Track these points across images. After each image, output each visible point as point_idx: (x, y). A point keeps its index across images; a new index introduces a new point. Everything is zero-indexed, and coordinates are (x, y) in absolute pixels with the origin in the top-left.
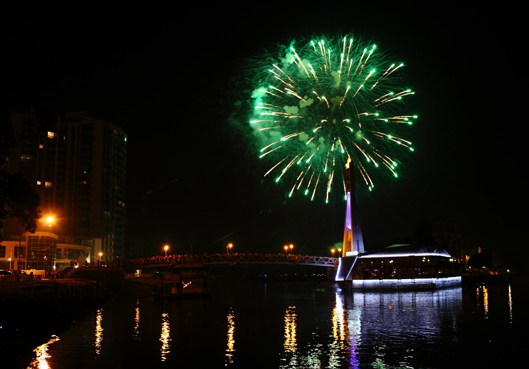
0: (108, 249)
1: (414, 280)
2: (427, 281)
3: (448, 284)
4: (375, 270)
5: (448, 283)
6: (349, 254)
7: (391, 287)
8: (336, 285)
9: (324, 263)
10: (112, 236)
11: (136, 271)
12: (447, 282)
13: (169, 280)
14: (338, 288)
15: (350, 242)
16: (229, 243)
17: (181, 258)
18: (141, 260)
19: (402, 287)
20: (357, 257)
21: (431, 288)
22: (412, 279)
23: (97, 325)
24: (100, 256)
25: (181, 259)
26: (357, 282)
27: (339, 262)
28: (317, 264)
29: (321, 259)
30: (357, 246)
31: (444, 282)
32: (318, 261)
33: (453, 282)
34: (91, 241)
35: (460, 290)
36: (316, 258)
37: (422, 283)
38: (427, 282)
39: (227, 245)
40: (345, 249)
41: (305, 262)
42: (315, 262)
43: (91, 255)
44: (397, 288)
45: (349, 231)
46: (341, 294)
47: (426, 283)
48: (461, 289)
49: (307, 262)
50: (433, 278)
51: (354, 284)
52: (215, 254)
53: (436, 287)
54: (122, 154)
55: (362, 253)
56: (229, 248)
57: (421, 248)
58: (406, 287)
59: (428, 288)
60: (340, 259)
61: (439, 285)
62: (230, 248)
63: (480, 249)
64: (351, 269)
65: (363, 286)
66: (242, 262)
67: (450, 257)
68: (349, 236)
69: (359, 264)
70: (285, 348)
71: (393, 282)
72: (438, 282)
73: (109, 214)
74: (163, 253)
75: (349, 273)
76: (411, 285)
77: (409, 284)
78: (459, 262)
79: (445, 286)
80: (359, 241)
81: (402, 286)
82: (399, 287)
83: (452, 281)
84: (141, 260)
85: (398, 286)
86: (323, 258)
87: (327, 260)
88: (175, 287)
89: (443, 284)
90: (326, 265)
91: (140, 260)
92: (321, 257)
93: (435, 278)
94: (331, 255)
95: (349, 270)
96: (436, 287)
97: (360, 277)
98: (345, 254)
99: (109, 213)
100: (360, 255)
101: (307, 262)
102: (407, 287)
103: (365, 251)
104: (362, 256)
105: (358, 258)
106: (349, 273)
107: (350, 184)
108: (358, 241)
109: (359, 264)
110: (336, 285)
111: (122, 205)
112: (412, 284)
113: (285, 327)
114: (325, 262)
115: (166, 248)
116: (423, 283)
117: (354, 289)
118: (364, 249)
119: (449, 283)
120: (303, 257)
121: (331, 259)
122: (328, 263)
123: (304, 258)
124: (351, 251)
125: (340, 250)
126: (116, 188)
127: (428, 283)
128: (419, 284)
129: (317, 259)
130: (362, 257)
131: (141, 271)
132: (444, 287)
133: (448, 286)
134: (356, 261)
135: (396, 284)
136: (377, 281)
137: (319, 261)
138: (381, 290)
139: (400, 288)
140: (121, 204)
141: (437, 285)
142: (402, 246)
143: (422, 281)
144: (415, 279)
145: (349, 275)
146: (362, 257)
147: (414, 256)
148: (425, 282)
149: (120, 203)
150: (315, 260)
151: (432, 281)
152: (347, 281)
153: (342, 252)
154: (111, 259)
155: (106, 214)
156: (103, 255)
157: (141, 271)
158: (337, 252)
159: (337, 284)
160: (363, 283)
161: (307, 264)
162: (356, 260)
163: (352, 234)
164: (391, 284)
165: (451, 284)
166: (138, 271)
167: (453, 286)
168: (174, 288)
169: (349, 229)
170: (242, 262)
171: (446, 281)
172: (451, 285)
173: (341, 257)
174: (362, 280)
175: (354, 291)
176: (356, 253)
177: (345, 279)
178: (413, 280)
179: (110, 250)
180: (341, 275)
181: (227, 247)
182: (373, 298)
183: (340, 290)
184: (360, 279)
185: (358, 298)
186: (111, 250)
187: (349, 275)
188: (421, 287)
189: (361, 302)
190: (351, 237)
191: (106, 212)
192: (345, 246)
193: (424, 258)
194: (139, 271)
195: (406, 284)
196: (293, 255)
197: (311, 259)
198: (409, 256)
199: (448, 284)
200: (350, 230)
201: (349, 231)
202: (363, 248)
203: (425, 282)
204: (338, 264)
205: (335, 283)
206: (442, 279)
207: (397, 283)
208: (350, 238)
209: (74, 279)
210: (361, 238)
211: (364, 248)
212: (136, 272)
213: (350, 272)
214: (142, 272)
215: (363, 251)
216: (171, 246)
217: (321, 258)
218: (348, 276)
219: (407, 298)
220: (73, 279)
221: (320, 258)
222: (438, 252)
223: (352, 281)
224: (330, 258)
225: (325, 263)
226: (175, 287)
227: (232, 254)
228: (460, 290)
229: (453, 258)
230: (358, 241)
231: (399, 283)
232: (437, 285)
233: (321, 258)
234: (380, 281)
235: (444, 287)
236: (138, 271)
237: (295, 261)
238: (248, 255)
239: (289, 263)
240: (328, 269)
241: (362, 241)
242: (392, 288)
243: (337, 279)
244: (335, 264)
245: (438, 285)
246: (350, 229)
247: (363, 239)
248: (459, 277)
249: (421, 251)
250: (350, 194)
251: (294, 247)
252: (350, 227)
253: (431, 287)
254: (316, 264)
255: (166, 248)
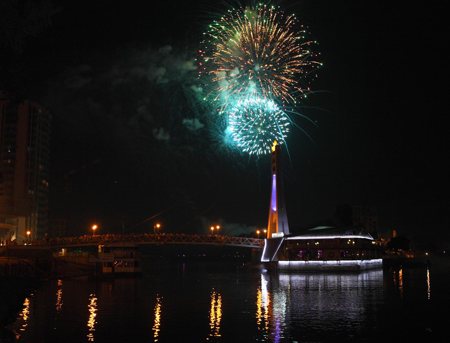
0: (32, 228)
1: (339, 262)
2: (352, 262)
3: (371, 266)
4: (300, 252)
5: (371, 265)
6: (274, 235)
7: (317, 268)
8: (262, 266)
9: (250, 244)
10: (35, 215)
11: (62, 250)
12: (370, 264)
13: (103, 259)
14: (264, 269)
15: (275, 224)
16: (157, 223)
17: (109, 237)
18: (69, 239)
19: (327, 269)
20: (283, 239)
21: (356, 270)
22: (337, 260)
23: (26, 302)
24: (28, 235)
25: (110, 238)
26: (283, 263)
27: (264, 243)
28: (242, 245)
29: (256, 241)
30: (282, 228)
31: (367, 264)
32: (244, 242)
33: (375, 264)
34: (15, 220)
35: (381, 273)
36: (242, 239)
37: (347, 265)
38: (353, 263)
39: (155, 225)
40: (270, 230)
41: (231, 243)
42: (241, 243)
43: (16, 234)
44: (322, 269)
45: (274, 213)
46: (266, 275)
47: (351, 264)
48: (382, 272)
49: (233, 243)
50: (358, 260)
51: (280, 265)
52: (143, 234)
53: (361, 269)
54: (46, 133)
55: (287, 234)
56: (156, 228)
57: (347, 231)
58: (331, 269)
59: (353, 270)
60: (265, 240)
61: (363, 267)
62: (212, 230)
63: (395, 232)
64: (277, 250)
65: (289, 267)
66: (169, 243)
67: (373, 239)
68: (274, 218)
69: (285, 245)
70: (265, 320)
71: (319, 263)
72: (362, 264)
73: (33, 193)
74: (92, 232)
75: (275, 254)
76: (336, 266)
77: (335, 265)
78: (380, 245)
79: (369, 268)
80: (284, 223)
81: (328, 268)
82: (324, 268)
83: (375, 263)
84: (69, 239)
85: (323, 268)
86: (248, 239)
87: (251, 241)
88: (107, 266)
89: (366, 266)
90: (251, 246)
91: (68, 239)
92: (247, 238)
93: (360, 260)
94: (255, 236)
95: (275, 251)
96: (361, 269)
97: (286, 258)
98: (271, 235)
99: (33, 192)
100: (286, 236)
101: (233, 243)
102: (332, 268)
103: (290, 233)
104: (288, 238)
105: (284, 239)
106: (275, 254)
107: (276, 168)
108: (283, 222)
109: (285, 245)
110: (262, 266)
111: (46, 184)
112: (337, 265)
113: (89, 318)
114: (250, 243)
115: (95, 227)
116: (348, 265)
117: (279, 269)
118: (289, 231)
119: (372, 265)
120: (229, 238)
121: (256, 240)
122: (253, 244)
123: (230, 239)
124: (276, 233)
125: (265, 231)
126: (40, 168)
127: (353, 264)
128: (344, 266)
129: (243, 241)
130: (289, 238)
131: (66, 249)
132: (368, 269)
133: (371, 268)
134: (282, 243)
135: (321, 266)
136: (303, 262)
137: (245, 242)
138: (307, 271)
139: (325, 269)
140: (45, 183)
141: (361, 267)
142: (313, 228)
143: (347, 263)
144: (341, 261)
145: (274, 256)
146: (289, 238)
147: (340, 238)
148: (350, 264)
149: (44, 182)
150: (241, 241)
151: (357, 263)
152: (273, 262)
153: (267, 234)
154: (34, 237)
155: (30, 193)
156: (30, 233)
157: (66, 249)
158: (262, 233)
159: (262, 265)
160: (289, 264)
161: (233, 244)
162: (282, 242)
163: (277, 216)
164: (316, 265)
165: (373, 266)
166: (63, 250)
167: (375, 268)
168: (106, 267)
169: (274, 211)
170: (169, 243)
171: (369, 263)
172: (373, 267)
173: (266, 239)
174: (288, 261)
175: (279, 272)
176: (282, 235)
177: (270, 260)
178: (338, 262)
179: (33, 229)
180: (266, 257)
181: (155, 227)
182: (298, 279)
183: (266, 271)
184: (286, 260)
185: (284, 278)
186: (35, 229)
187: (274, 256)
188: (346, 269)
189: (287, 284)
190: (276, 219)
191: (30, 191)
192: (270, 227)
193: (350, 241)
194: (64, 250)
195: (331, 266)
196: (220, 236)
197: (237, 240)
198: (335, 238)
199: (371, 266)
200: (275, 212)
201: (274, 213)
202: (288, 229)
203: (350, 264)
204: (264, 245)
205: (261, 264)
206: (366, 261)
207: (323, 265)
208: (276, 220)
209: (5, 257)
210: (286, 220)
211: (289, 230)
212: (62, 251)
213: (276, 253)
214: (67, 252)
215: (288, 233)
216: (99, 226)
217: (237, 239)
218: (274, 257)
219: (332, 279)
220: (3, 257)
221: (245, 239)
222: (362, 235)
223: (278, 261)
224: (255, 239)
225: (251, 244)
226: (107, 266)
227: (160, 234)
228: (381, 273)
229: (375, 241)
230: (283, 222)
231: (325, 265)
232: (361, 267)
233: (247, 239)
234: (306, 263)
235: (368, 269)
236: (63, 250)
237: (221, 242)
238: (175, 235)
239: (216, 244)
240: (253, 250)
241: (287, 223)
242: (318, 269)
243: (262, 260)
244: (260, 245)
245: (362, 267)
246: (275, 211)
247: (288, 221)
248: (380, 259)
249: (347, 233)
250: (276, 176)
251: (160, 227)
252: (275, 209)
253: (356, 269)
254: (242, 245)
255: (95, 227)
